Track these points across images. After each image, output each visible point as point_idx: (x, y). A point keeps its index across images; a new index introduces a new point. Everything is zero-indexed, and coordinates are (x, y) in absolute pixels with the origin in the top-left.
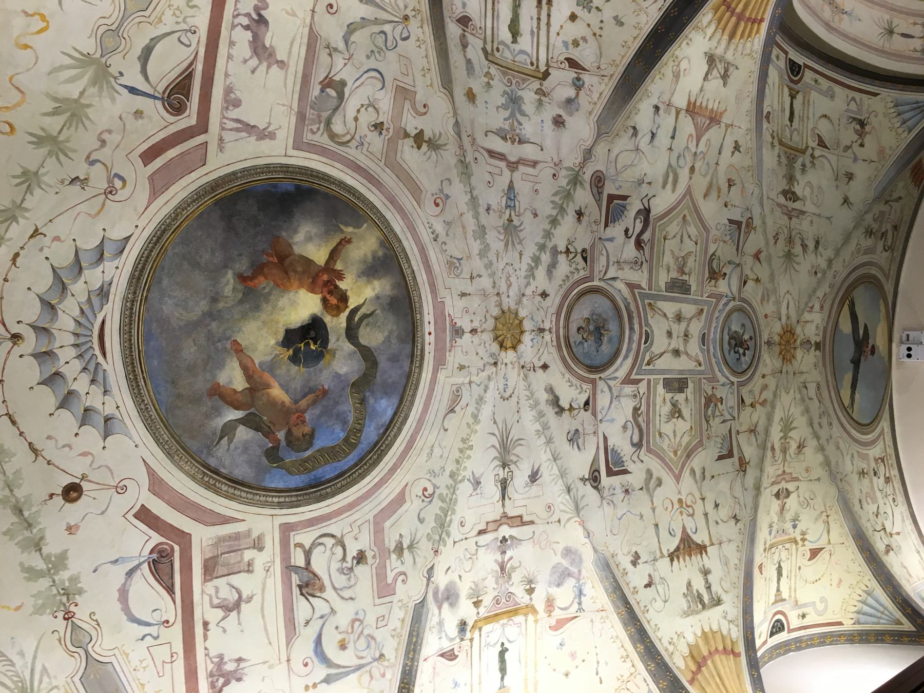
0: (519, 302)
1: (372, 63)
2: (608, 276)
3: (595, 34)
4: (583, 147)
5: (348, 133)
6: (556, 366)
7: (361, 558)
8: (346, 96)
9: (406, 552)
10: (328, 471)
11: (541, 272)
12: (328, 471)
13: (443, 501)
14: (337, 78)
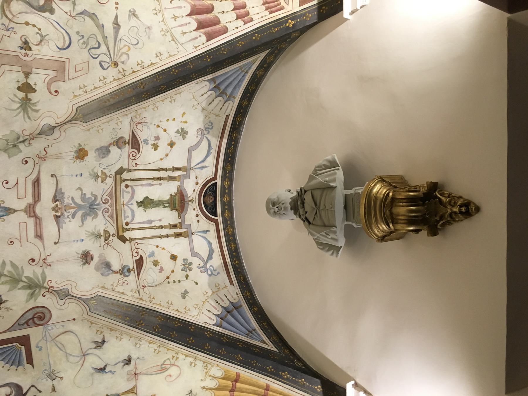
1: (75, 38)
3: (168, 278)
4: (69, 287)
5: (14, 16)
8: (43, 14)
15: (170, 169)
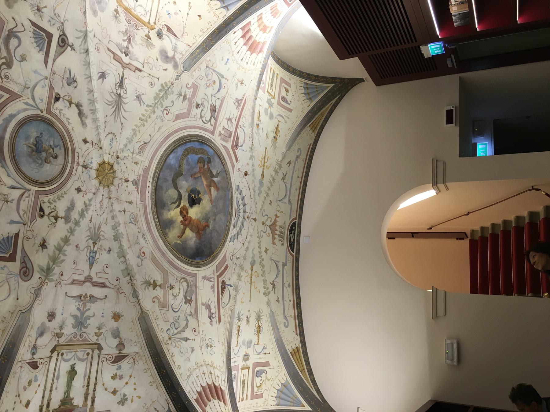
0: (98, 190)
1: (177, 314)
2: (22, 191)
6: (77, 138)
7: (198, 106)
9: (183, 95)
10: (196, 145)
11: (79, 206)
12: (196, 145)
13: (161, 103)
14: (188, 304)
15: (94, 394)
